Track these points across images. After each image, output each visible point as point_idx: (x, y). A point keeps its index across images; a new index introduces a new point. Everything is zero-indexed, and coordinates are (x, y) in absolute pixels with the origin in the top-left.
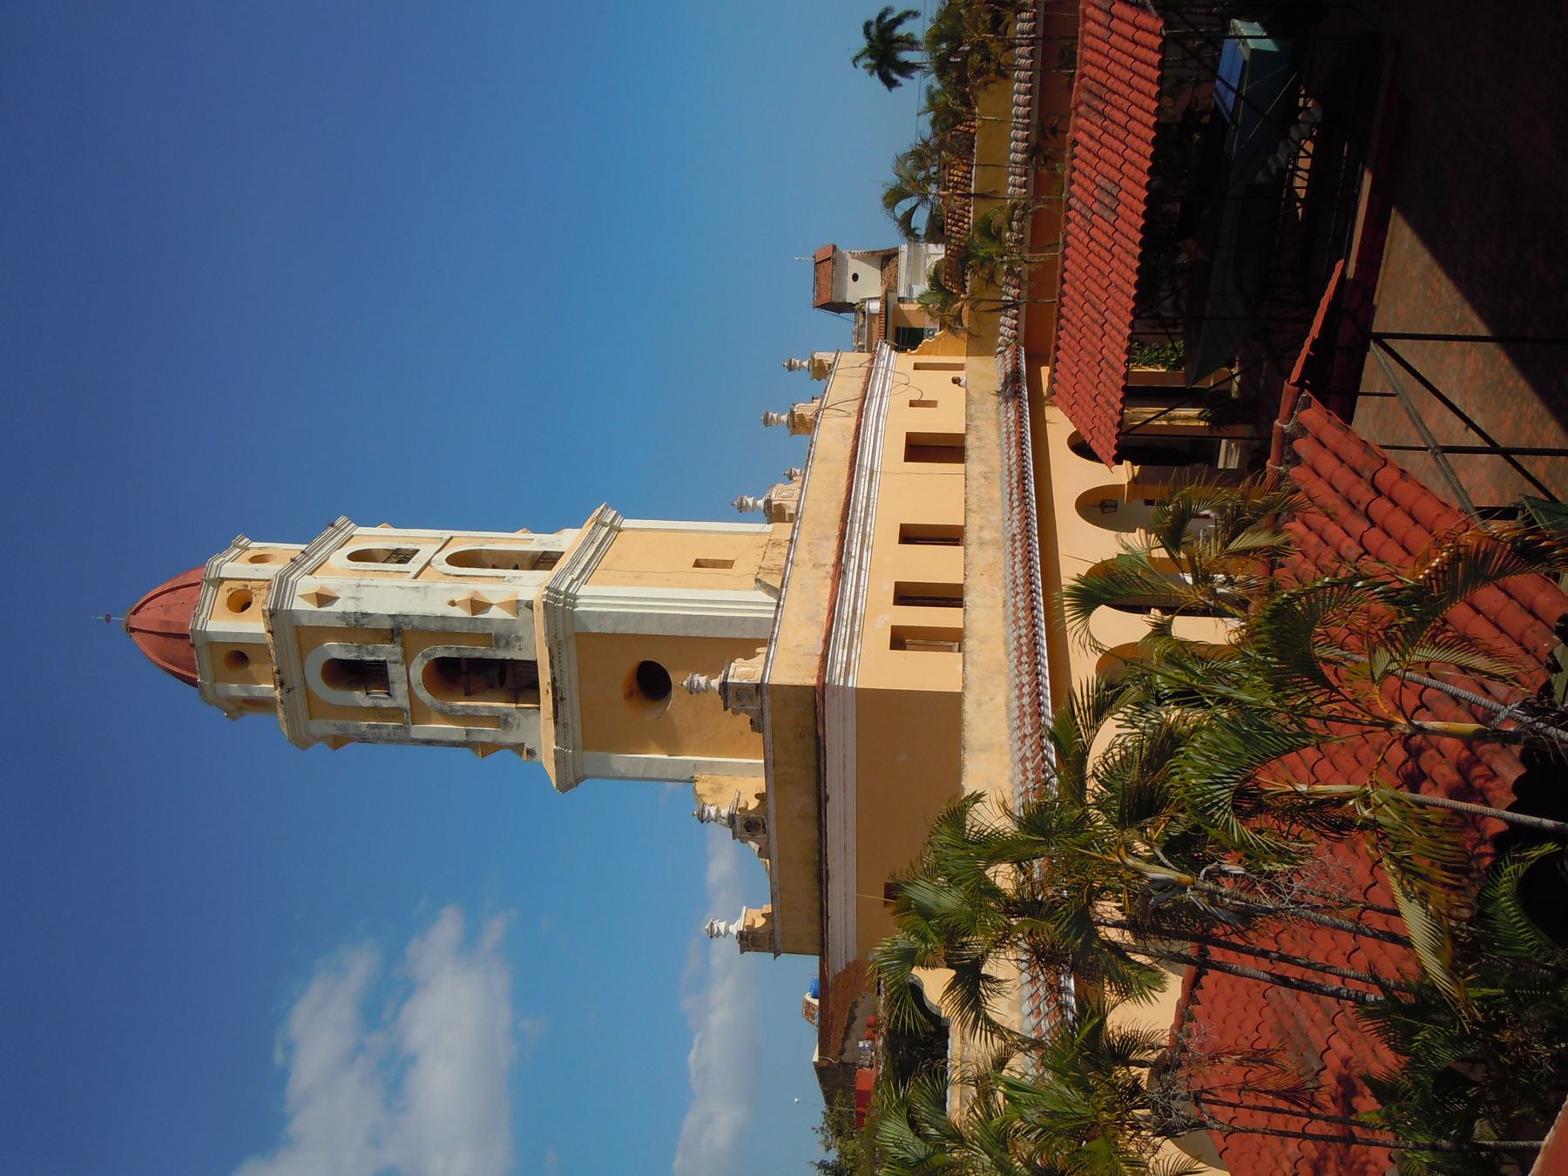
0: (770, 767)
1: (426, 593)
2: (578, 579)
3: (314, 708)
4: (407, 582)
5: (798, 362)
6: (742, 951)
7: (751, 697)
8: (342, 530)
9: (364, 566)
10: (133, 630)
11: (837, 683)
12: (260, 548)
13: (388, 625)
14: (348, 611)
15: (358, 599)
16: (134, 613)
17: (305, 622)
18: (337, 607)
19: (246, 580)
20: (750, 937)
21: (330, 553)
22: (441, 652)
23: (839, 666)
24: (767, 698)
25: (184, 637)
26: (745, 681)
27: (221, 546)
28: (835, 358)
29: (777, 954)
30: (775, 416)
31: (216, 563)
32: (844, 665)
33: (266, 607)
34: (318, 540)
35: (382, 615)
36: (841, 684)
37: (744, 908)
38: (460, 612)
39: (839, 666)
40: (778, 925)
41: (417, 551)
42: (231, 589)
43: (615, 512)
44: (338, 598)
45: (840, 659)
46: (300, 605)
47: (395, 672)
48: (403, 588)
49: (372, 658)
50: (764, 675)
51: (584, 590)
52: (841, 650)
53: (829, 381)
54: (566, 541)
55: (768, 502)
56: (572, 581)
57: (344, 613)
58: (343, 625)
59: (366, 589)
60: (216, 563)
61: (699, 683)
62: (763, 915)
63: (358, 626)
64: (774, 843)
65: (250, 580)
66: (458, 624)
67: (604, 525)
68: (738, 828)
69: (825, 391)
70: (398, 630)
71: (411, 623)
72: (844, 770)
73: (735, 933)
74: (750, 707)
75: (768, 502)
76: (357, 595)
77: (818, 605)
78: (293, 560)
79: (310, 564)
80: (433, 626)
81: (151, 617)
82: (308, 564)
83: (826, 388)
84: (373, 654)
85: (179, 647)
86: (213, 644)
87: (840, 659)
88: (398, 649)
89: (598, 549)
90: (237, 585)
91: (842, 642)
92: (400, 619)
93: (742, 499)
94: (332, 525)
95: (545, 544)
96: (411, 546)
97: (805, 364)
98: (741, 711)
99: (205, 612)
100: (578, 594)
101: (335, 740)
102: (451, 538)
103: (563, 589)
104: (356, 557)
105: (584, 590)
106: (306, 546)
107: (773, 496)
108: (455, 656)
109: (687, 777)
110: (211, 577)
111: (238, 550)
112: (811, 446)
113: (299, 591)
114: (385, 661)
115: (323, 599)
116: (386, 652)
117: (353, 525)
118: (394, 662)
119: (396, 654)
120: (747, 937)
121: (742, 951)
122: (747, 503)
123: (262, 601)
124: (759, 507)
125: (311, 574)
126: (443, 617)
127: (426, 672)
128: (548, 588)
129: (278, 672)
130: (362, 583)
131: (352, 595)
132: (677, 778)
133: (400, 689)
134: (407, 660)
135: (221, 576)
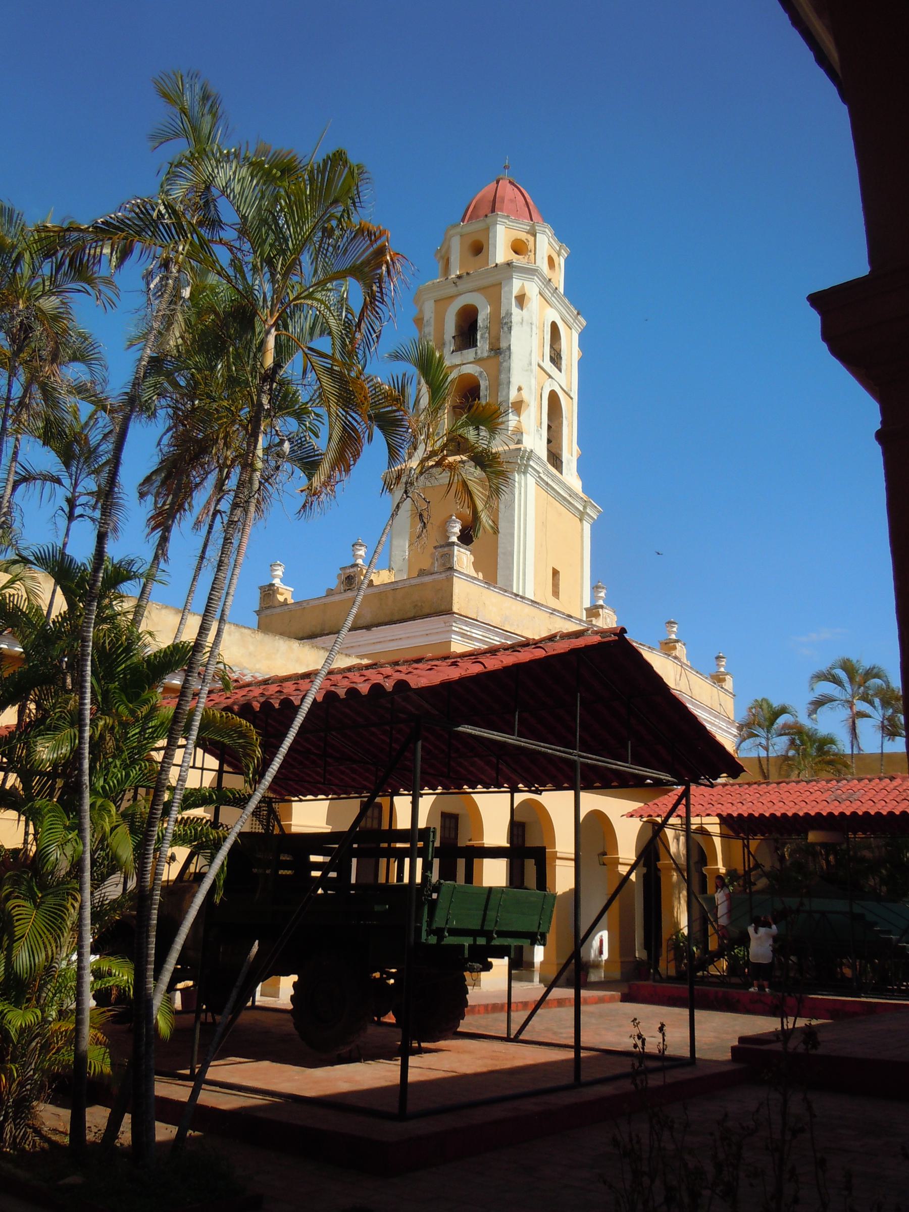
0: (392, 587)
1: (527, 370)
2: (540, 477)
3: (442, 302)
4: (536, 359)
5: (723, 663)
6: (261, 588)
7: (444, 565)
8: (575, 321)
9: (547, 331)
10: (498, 182)
11: (454, 624)
12: (559, 264)
13: (503, 345)
14: (513, 317)
15: (522, 324)
16: (510, 182)
17: (505, 290)
18: (515, 310)
19: (535, 251)
20: (271, 592)
21: (556, 309)
22: (483, 384)
23: (468, 629)
24: (443, 575)
25: (493, 211)
26: (455, 559)
27: (561, 235)
28: (727, 691)
29: (258, 613)
30: (675, 629)
31: (547, 230)
32: (469, 633)
33: (514, 261)
34: (566, 301)
35: (510, 341)
36: (453, 628)
37: (293, 590)
38: (513, 395)
39: (468, 629)
40: (278, 610)
41: (560, 370)
42: (528, 241)
43: (596, 518)
44: (522, 309)
45: (473, 631)
46: (517, 285)
47: (470, 354)
48: (530, 355)
49: (479, 337)
50: (460, 573)
51: (531, 480)
52: (481, 633)
53: (706, 678)
54: (571, 477)
55: (602, 607)
56: (538, 472)
57: (511, 314)
58: (503, 315)
59: (529, 330)
60: (547, 230)
61: (454, 527)
62: (286, 599)
63: (502, 324)
64: (337, 598)
65: (535, 254)
66: (504, 393)
67: (585, 507)
68: (348, 571)
69: (697, 672)
70: (499, 352)
71: (504, 361)
72: (390, 640)
73: (274, 582)
74: (436, 565)
75: (602, 607)
76: (524, 323)
77: (518, 625)
78: (550, 280)
79: (548, 294)
80: (503, 376)
81: (507, 191)
82: (547, 291)
83: (701, 675)
84: (482, 337)
85: (487, 209)
86: (488, 231)
87: (473, 631)
88: (486, 354)
89: (565, 499)
90: (531, 246)
91: (487, 635)
92: (507, 353)
93: (603, 588)
94: (578, 314)
95: (569, 464)
96: (564, 367)
97: (722, 669)
98: (434, 559)
99: (511, 224)
100: (528, 475)
101: (419, 319)
102: (571, 398)
103: (531, 463)
104: (554, 327)
105: (531, 480)
106: (562, 292)
107: (607, 611)
108: (481, 394)
109: (393, 565)
110: (537, 228)
111: (558, 248)
112: (649, 648)
113: (526, 283)
114: (476, 346)
115: (521, 300)
116: (483, 345)
117: (566, 255)
118: (476, 353)
119: (482, 353)
120: (271, 590)
121: (261, 588)
122: (601, 592)
123: (518, 260)
124: (597, 601)
125: (540, 293)
126: (509, 383)
127: (470, 376)
128: (532, 451)
129: (468, 274)
130: (534, 327)
131: (524, 320)
132: (392, 559)
133: (457, 359)
134: (478, 361)
135: (538, 234)
